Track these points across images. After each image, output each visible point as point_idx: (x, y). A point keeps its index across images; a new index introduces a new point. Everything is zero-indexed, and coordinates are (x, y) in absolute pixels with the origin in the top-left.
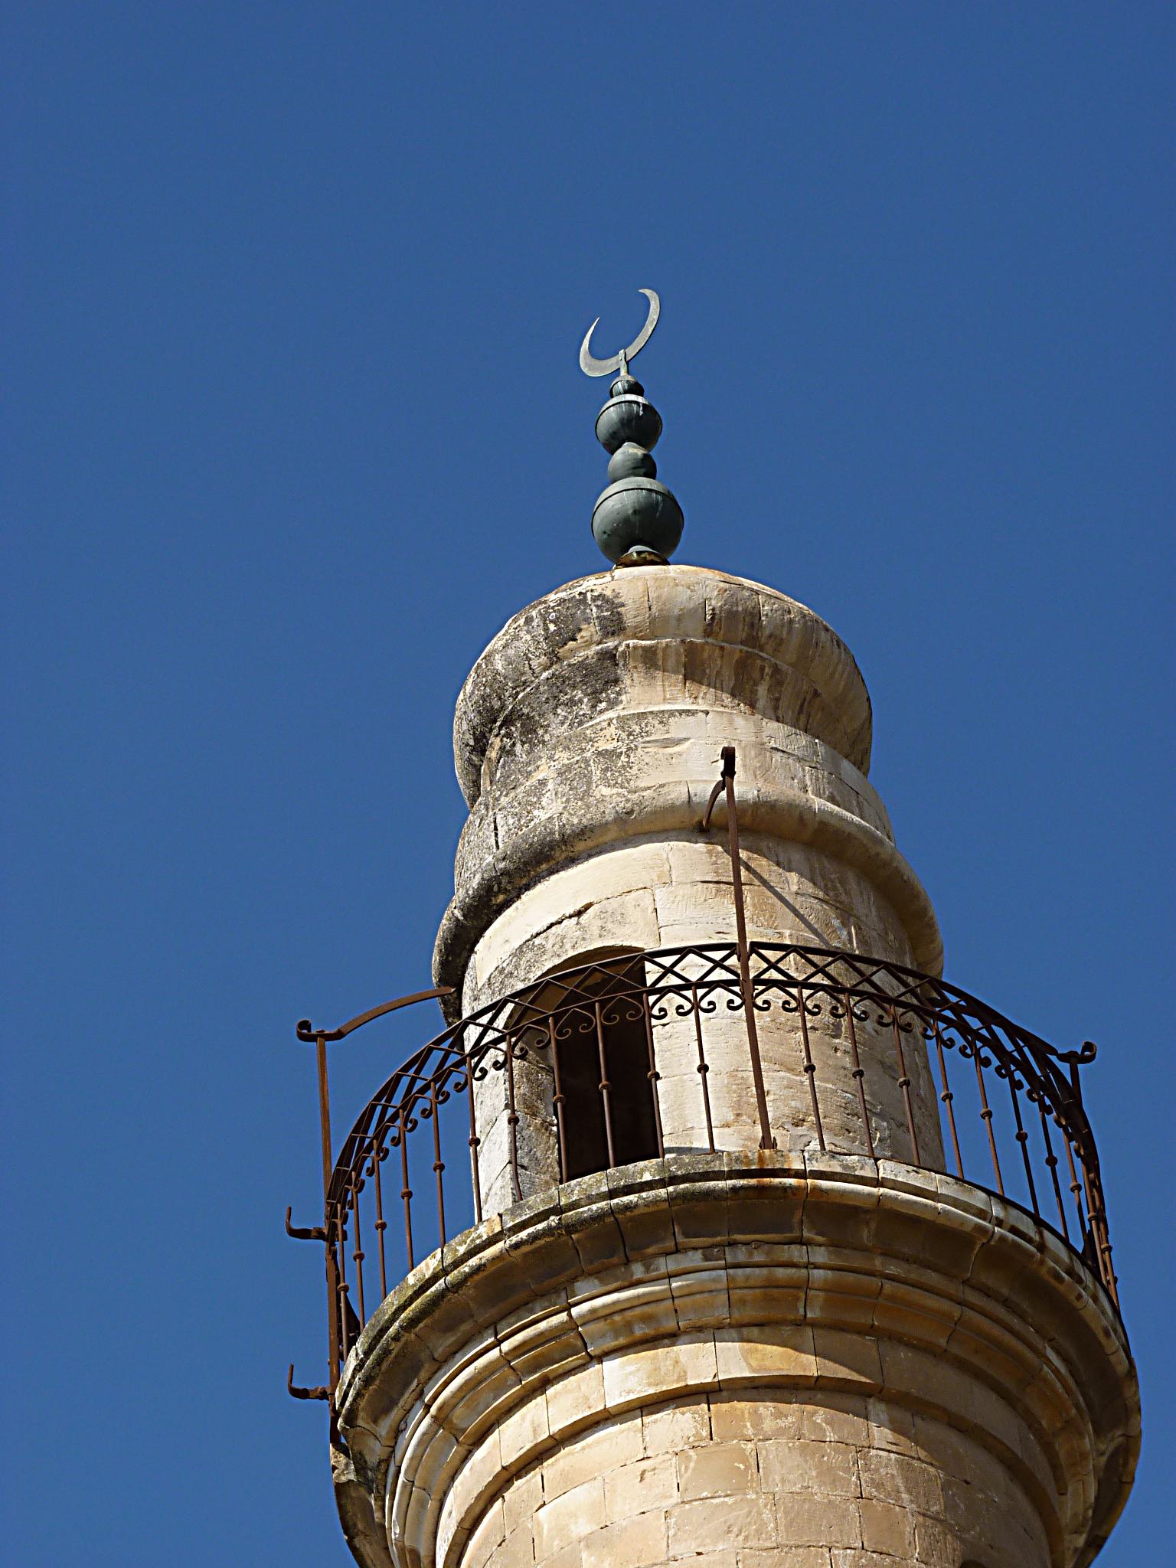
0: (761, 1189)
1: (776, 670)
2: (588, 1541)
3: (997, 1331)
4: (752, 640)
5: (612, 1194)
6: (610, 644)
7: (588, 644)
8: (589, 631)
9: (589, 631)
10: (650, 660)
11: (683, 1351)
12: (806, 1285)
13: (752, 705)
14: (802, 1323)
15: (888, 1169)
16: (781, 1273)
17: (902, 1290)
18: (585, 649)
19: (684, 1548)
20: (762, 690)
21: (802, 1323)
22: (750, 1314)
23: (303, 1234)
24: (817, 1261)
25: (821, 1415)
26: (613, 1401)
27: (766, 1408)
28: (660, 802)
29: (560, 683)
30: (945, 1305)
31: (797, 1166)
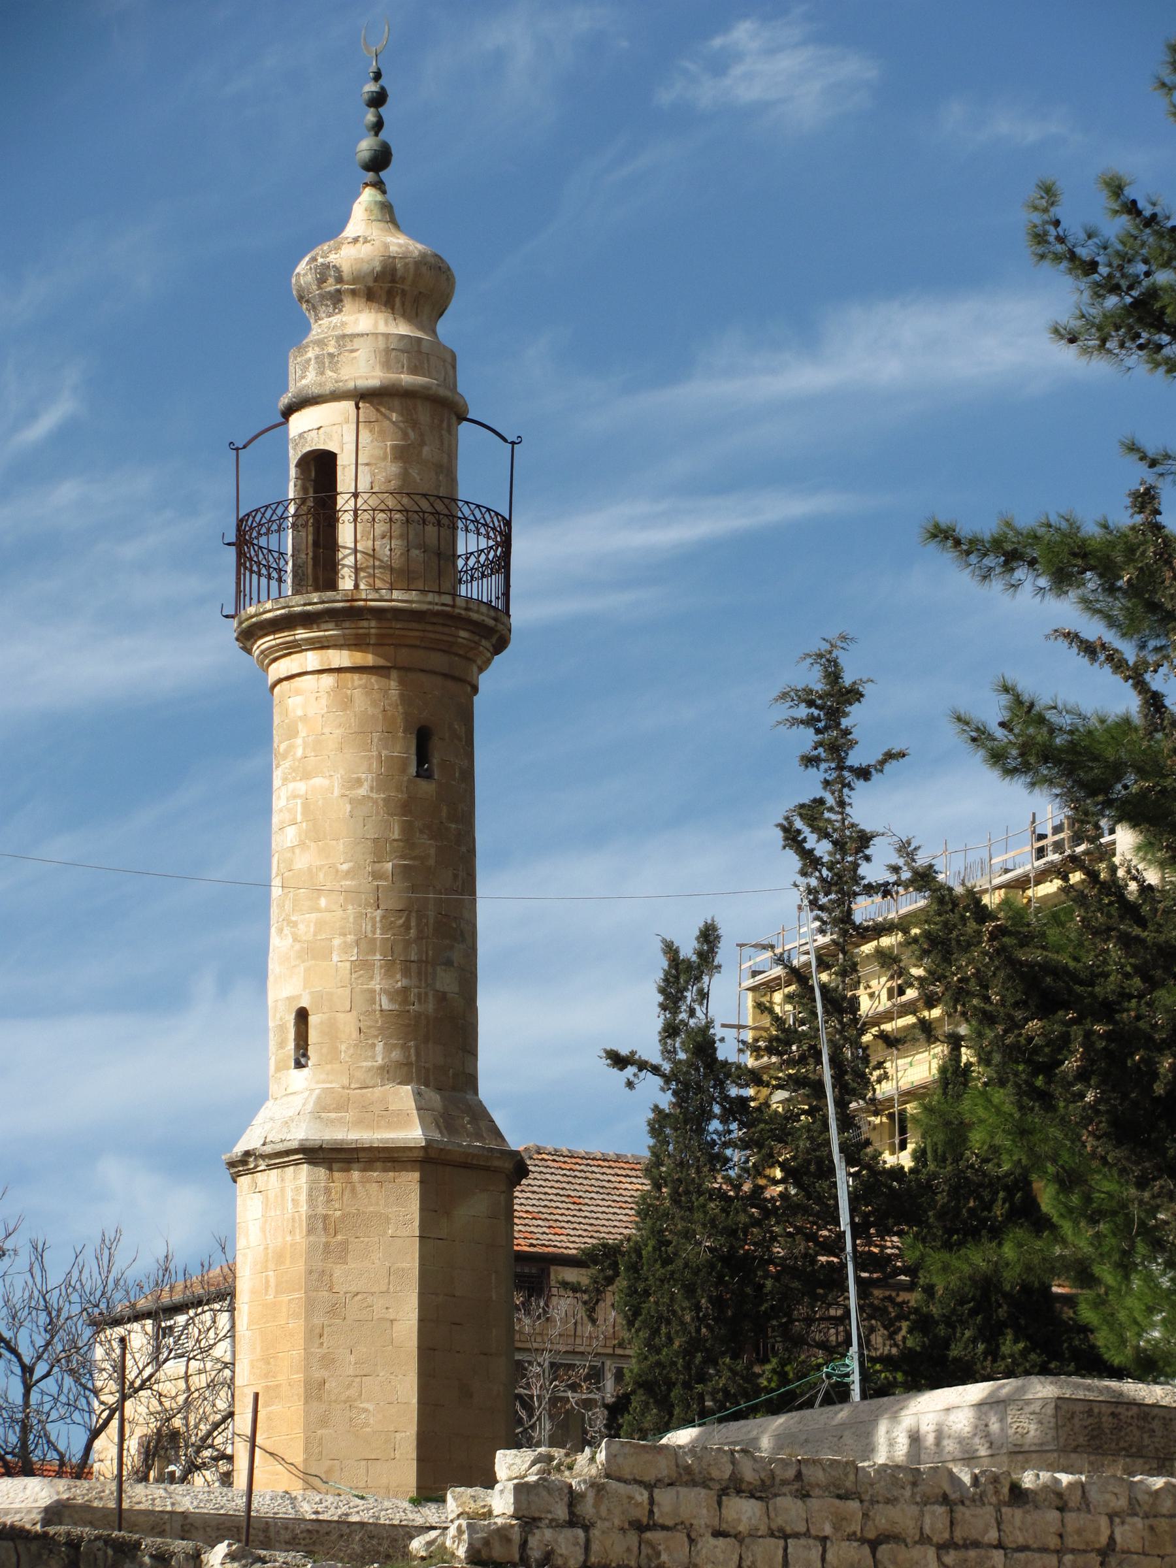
0: (352, 608)
1: (403, 290)
2: (300, 718)
3: (438, 636)
4: (393, 281)
5: (305, 605)
6: (338, 287)
7: (331, 285)
8: (331, 280)
9: (331, 280)
10: (353, 293)
11: (331, 652)
12: (368, 635)
13: (393, 309)
14: (368, 644)
15: (396, 594)
16: (361, 631)
17: (402, 632)
18: (331, 286)
19: (327, 730)
20: (398, 300)
21: (368, 644)
22: (351, 642)
23: (229, 544)
24: (371, 626)
25: (373, 679)
26: (309, 669)
27: (356, 676)
28: (345, 388)
29: (323, 297)
30: (417, 634)
31: (364, 597)
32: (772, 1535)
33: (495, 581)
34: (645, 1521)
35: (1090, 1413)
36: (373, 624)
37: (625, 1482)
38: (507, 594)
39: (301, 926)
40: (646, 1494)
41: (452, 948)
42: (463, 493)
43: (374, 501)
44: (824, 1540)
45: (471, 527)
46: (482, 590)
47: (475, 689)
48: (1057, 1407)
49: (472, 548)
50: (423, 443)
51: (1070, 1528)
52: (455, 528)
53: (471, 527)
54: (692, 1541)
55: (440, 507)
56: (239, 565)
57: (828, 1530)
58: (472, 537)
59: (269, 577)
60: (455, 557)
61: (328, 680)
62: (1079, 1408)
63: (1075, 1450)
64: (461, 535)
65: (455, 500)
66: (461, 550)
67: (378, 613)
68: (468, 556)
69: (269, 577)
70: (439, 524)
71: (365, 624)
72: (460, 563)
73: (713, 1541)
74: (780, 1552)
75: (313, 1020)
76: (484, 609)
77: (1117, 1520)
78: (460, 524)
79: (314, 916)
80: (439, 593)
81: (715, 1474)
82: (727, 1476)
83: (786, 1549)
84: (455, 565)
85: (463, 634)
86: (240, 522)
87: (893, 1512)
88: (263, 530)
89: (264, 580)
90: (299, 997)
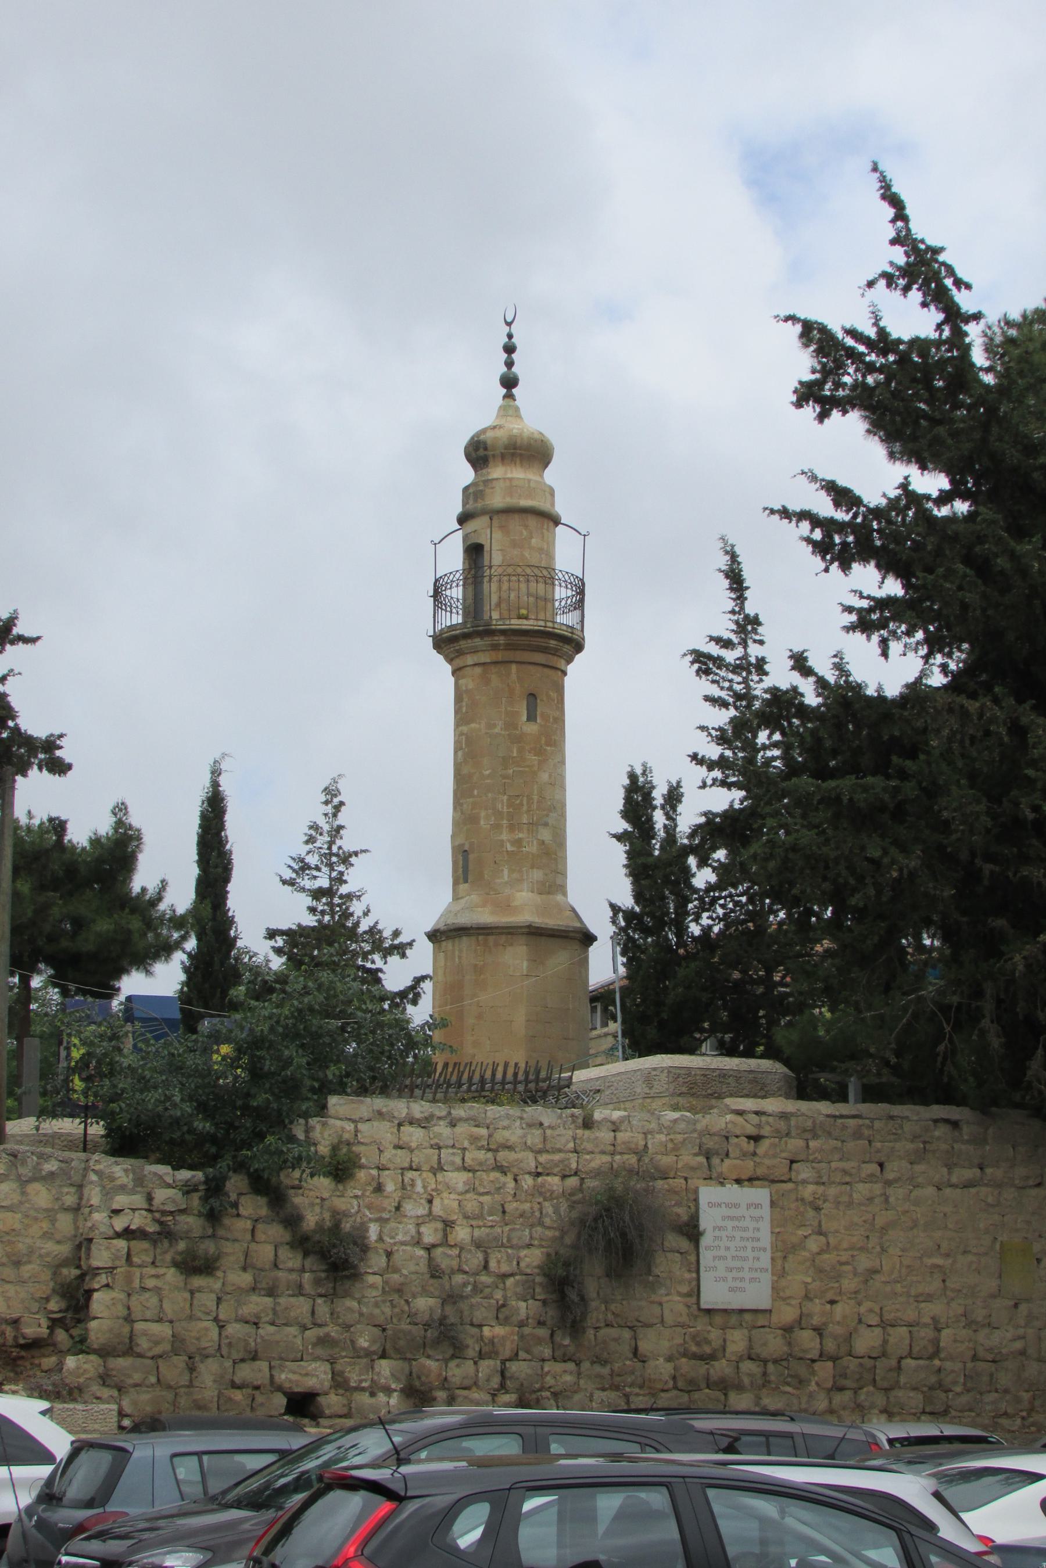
8: (481, 450)
32: (432, 1147)
33: (578, 612)
34: (352, 1141)
35: (689, 1075)
36: (502, 638)
37: (341, 1119)
38: (582, 621)
39: (465, 806)
40: (352, 1126)
41: (547, 816)
42: (559, 566)
43: (500, 570)
44: (465, 1149)
45: (563, 584)
46: (568, 619)
47: (565, 673)
48: (669, 1072)
49: (563, 596)
50: (531, 538)
51: (619, 1141)
52: (553, 584)
53: (563, 584)
54: (381, 1151)
55: (545, 573)
56: (435, 605)
57: (466, 1144)
58: (563, 590)
59: (451, 612)
60: (554, 600)
61: (478, 670)
62: (683, 1072)
63: (680, 1095)
64: (557, 588)
65: (554, 570)
66: (557, 597)
67: (503, 632)
68: (561, 600)
69: (451, 612)
70: (546, 583)
71: (496, 638)
72: (557, 604)
73: (394, 1151)
74: (436, 1157)
75: (471, 857)
76: (564, 628)
77: (649, 1136)
78: (557, 582)
79: (471, 800)
80: (537, 620)
81: (396, 1114)
82: (404, 1115)
83: (439, 1156)
84: (554, 605)
85: (552, 642)
86: (436, 580)
87: (506, 1134)
88: (454, 584)
89: (448, 614)
90: (463, 845)
